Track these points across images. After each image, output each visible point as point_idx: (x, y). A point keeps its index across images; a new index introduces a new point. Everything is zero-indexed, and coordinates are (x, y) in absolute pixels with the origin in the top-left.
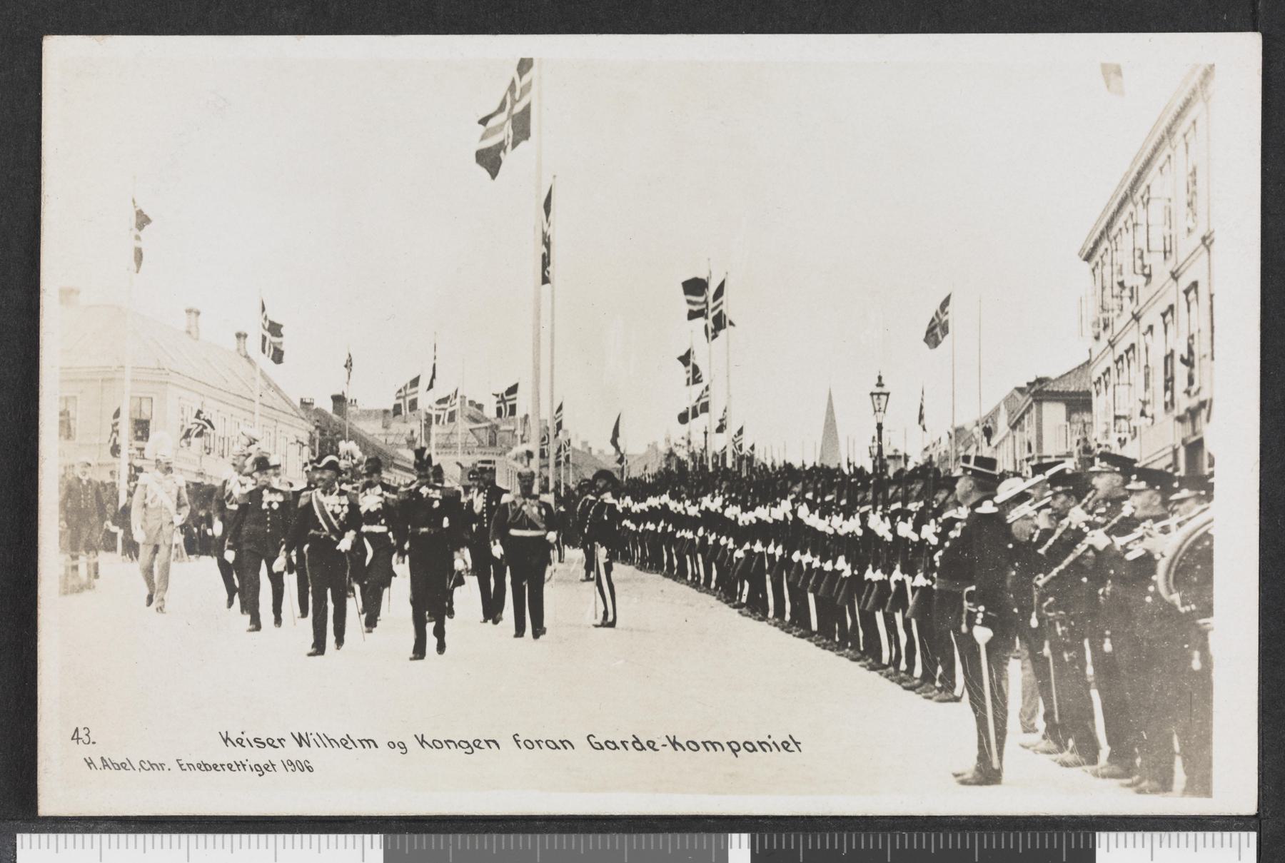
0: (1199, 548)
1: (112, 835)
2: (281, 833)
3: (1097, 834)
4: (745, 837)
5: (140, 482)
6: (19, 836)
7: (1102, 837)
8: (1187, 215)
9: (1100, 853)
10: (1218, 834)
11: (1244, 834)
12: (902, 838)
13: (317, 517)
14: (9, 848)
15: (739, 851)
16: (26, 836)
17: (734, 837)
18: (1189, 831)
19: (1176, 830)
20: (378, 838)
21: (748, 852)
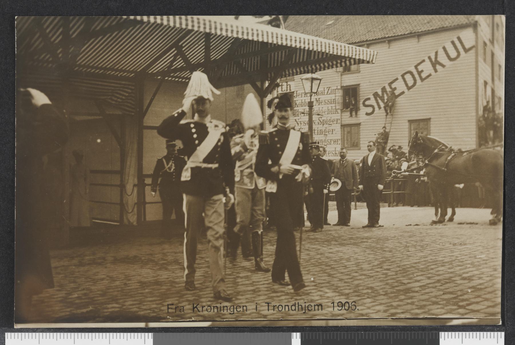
0: (236, 229)
1: (44, 333)
2: (83, 332)
3: (440, 333)
4: (299, 334)
5: (298, 104)
6: (6, 334)
7: (442, 334)
8: (196, 96)
9: (441, 341)
10: (489, 333)
11: (499, 333)
12: (379, 334)
13: (205, 168)
14: (2, 338)
15: (296, 340)
16: (9, 334)
17: (294, 334)
18: (477, 331)
19: (472, 331)
20: (150, 334)
21: (300, 340)
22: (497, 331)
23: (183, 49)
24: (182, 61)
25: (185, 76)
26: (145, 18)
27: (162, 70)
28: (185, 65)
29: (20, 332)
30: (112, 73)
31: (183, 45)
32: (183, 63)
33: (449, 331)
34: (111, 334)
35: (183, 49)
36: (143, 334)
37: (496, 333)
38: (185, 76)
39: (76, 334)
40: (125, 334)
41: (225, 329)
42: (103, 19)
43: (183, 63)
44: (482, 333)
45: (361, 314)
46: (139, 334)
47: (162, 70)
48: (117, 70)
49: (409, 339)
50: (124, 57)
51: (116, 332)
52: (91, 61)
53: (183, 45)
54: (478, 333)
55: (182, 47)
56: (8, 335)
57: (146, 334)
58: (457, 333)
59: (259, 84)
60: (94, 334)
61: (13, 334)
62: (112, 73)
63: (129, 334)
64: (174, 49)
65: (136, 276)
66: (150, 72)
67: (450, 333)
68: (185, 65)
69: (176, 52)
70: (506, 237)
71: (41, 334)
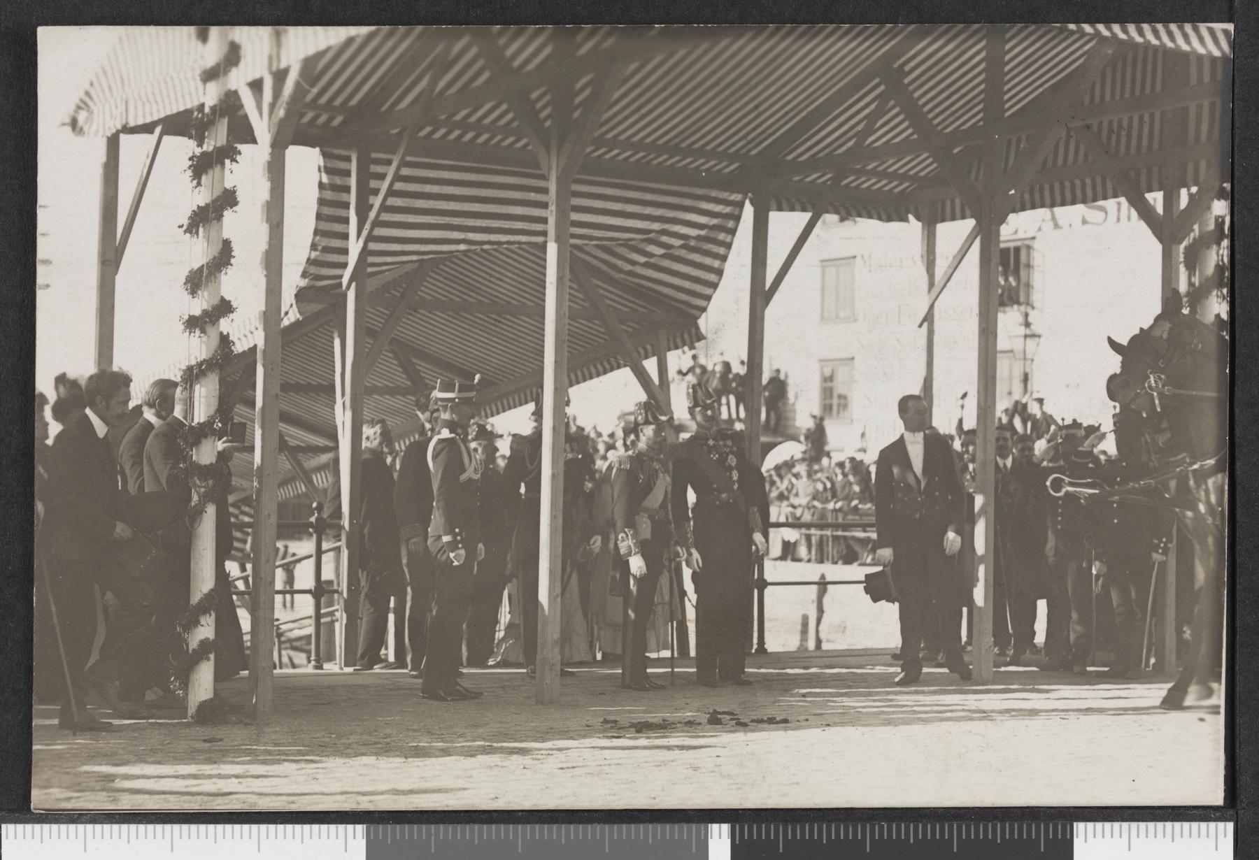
1: (96, 826)
3: (1075, 824)
4: (726, 828)
7: (1080, 828)
15: (719, 841)
16: (11, 827)
19: (1123, 820)
20: (360, 829)
22: (1214, 821)
23: (906, 81)
24: (906, 123)
25: (912, 172)
26: (1087, 28)
27: (826, 151)
28: (915, 136)
29: (1083, 821)
30: (437, 135)
31: (907, 68)
32: (910, 131)
33: (1098, 821)
34: (263, 827)
35: (906, 81)
36: (341, 827)
37: (1212, 825)
38: (912, 172)
39: (176, 827)
40: (298, 827)
41: (545, 815)
42: (946, 31)
43: (910, 131)
44: (1177, 825)
45: (197, 779)
46: (333, 827)
47: (826, 151)
48: (688, 151)
49: (650, 841)
50: (714, 113)
51: (275, 822)
52: (719, 140)
53: (907, 68)
54: (1169, 825)
55: (901, 73)
56: (9, 829)
57: (350, 827)
58: (1116, 825)
59: (1156, 199)
60: (220, 827)
61: (29, 827)
62: (437, 135)
63: (307, 827)
64: (877, 80)
65: (1001, 712)
66: (790, 157)
67: (1099, 825)
68: (915, 136)
69: (882, 88)
70: (1238, 587)
71: (90, 827)
